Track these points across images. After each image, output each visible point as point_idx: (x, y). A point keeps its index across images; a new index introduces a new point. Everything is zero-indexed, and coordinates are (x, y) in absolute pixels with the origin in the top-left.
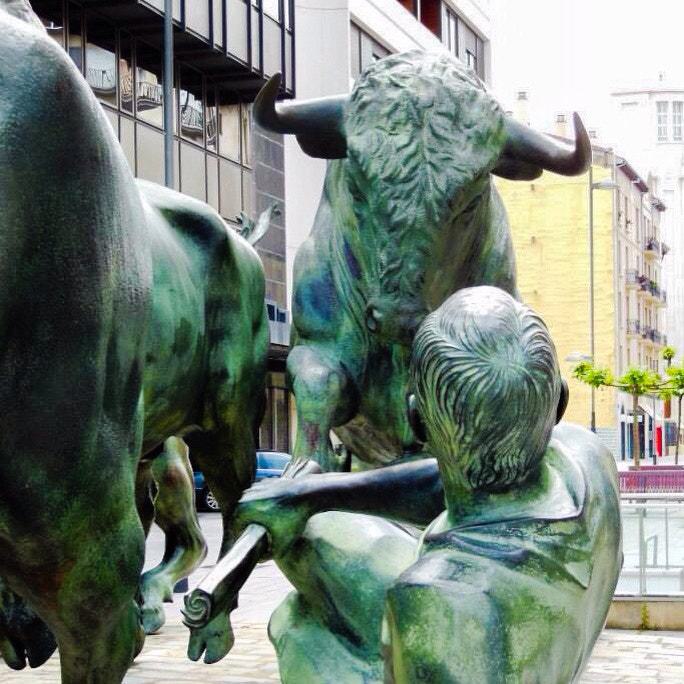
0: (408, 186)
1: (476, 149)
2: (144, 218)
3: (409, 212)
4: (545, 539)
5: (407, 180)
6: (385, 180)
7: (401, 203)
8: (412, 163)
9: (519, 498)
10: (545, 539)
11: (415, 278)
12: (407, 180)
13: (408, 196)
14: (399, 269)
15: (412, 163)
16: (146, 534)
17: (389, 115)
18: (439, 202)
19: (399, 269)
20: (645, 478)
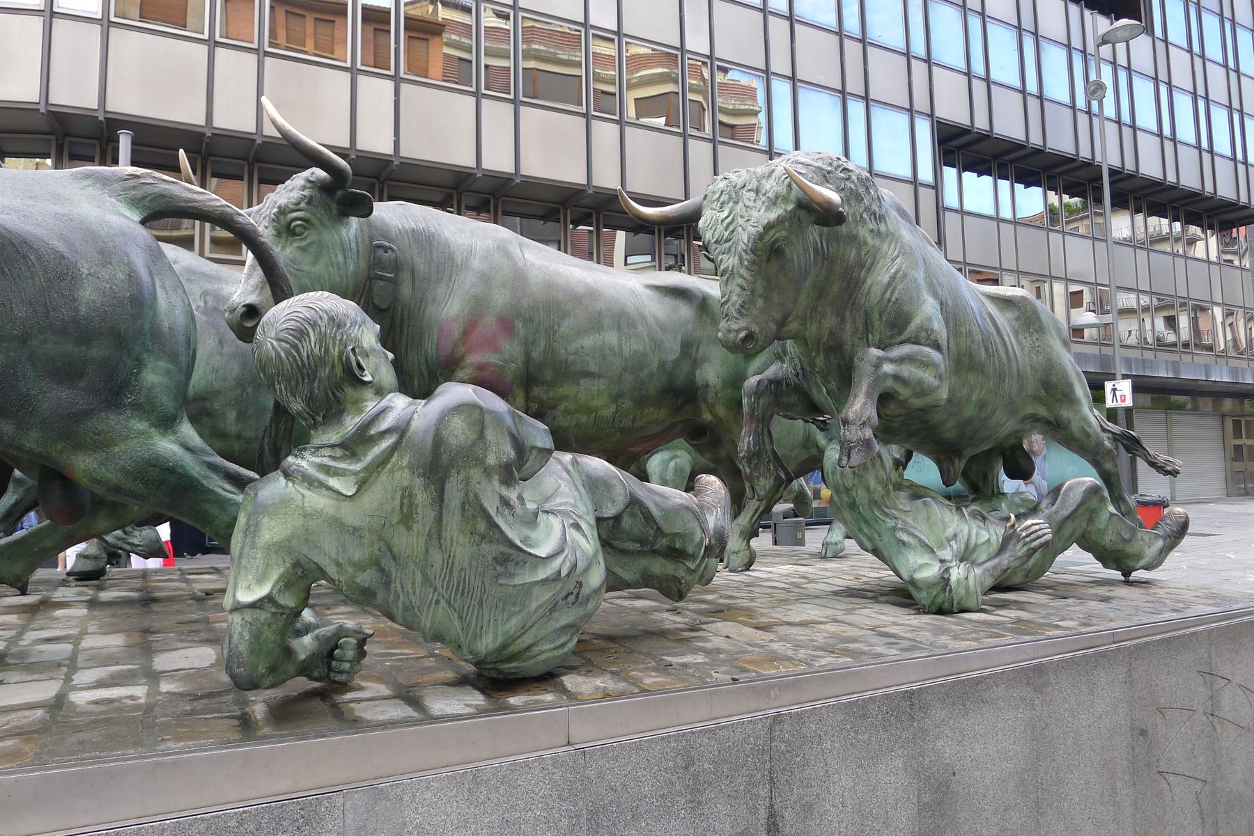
0: (727, 245)
1: (768, 209)
2: (155, 315)
3: (729, 261)
4: (318, 460)
5: (728, 240)
6: (716, 242)
7: (725, 257)
8: (731, 228)
9: (287, 696)
10: (318, 460)
11: (737, 306)
12: (728, 240)
13: (729, 251)
14: (727, 301)
15: (731, 228)
16: (268, 688)
17: (718, 199)
18: (745, 251)
19: (727, 301)
20: (362, 643)
